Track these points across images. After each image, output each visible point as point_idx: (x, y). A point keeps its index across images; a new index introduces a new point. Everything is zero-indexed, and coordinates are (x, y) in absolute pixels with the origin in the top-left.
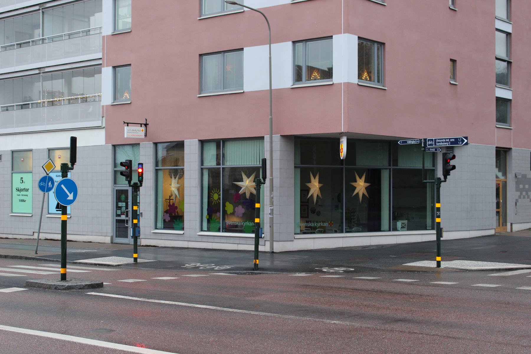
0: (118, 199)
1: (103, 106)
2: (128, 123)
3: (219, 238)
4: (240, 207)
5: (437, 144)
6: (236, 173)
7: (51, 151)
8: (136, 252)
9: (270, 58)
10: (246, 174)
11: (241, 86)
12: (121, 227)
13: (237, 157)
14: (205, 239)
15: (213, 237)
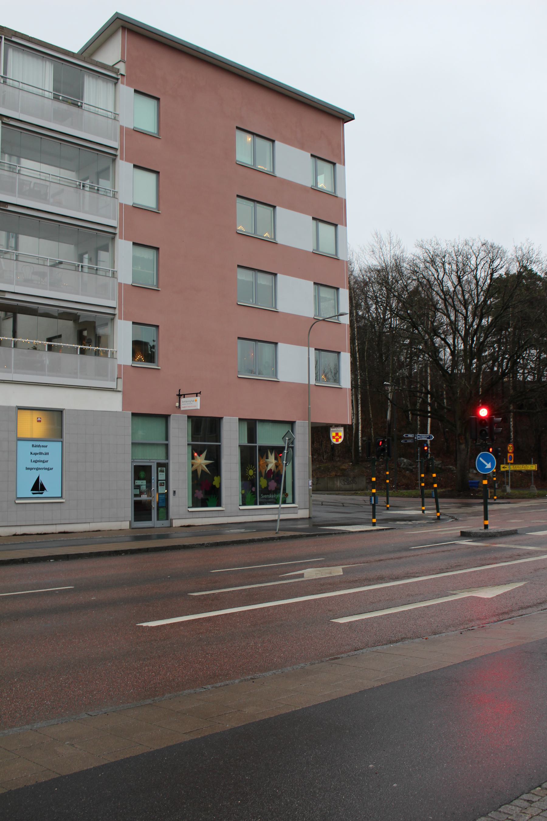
0: (137, 477)
1: (119, 366)
2: (184, 395)
4: (273, 481)
6: (264, 451)
7: (60, 413)
8: (374, 518)
9: (309, 358)
11: (276, 376)
12: (141, 510)
13: (267, 437)
14: (247, 513)
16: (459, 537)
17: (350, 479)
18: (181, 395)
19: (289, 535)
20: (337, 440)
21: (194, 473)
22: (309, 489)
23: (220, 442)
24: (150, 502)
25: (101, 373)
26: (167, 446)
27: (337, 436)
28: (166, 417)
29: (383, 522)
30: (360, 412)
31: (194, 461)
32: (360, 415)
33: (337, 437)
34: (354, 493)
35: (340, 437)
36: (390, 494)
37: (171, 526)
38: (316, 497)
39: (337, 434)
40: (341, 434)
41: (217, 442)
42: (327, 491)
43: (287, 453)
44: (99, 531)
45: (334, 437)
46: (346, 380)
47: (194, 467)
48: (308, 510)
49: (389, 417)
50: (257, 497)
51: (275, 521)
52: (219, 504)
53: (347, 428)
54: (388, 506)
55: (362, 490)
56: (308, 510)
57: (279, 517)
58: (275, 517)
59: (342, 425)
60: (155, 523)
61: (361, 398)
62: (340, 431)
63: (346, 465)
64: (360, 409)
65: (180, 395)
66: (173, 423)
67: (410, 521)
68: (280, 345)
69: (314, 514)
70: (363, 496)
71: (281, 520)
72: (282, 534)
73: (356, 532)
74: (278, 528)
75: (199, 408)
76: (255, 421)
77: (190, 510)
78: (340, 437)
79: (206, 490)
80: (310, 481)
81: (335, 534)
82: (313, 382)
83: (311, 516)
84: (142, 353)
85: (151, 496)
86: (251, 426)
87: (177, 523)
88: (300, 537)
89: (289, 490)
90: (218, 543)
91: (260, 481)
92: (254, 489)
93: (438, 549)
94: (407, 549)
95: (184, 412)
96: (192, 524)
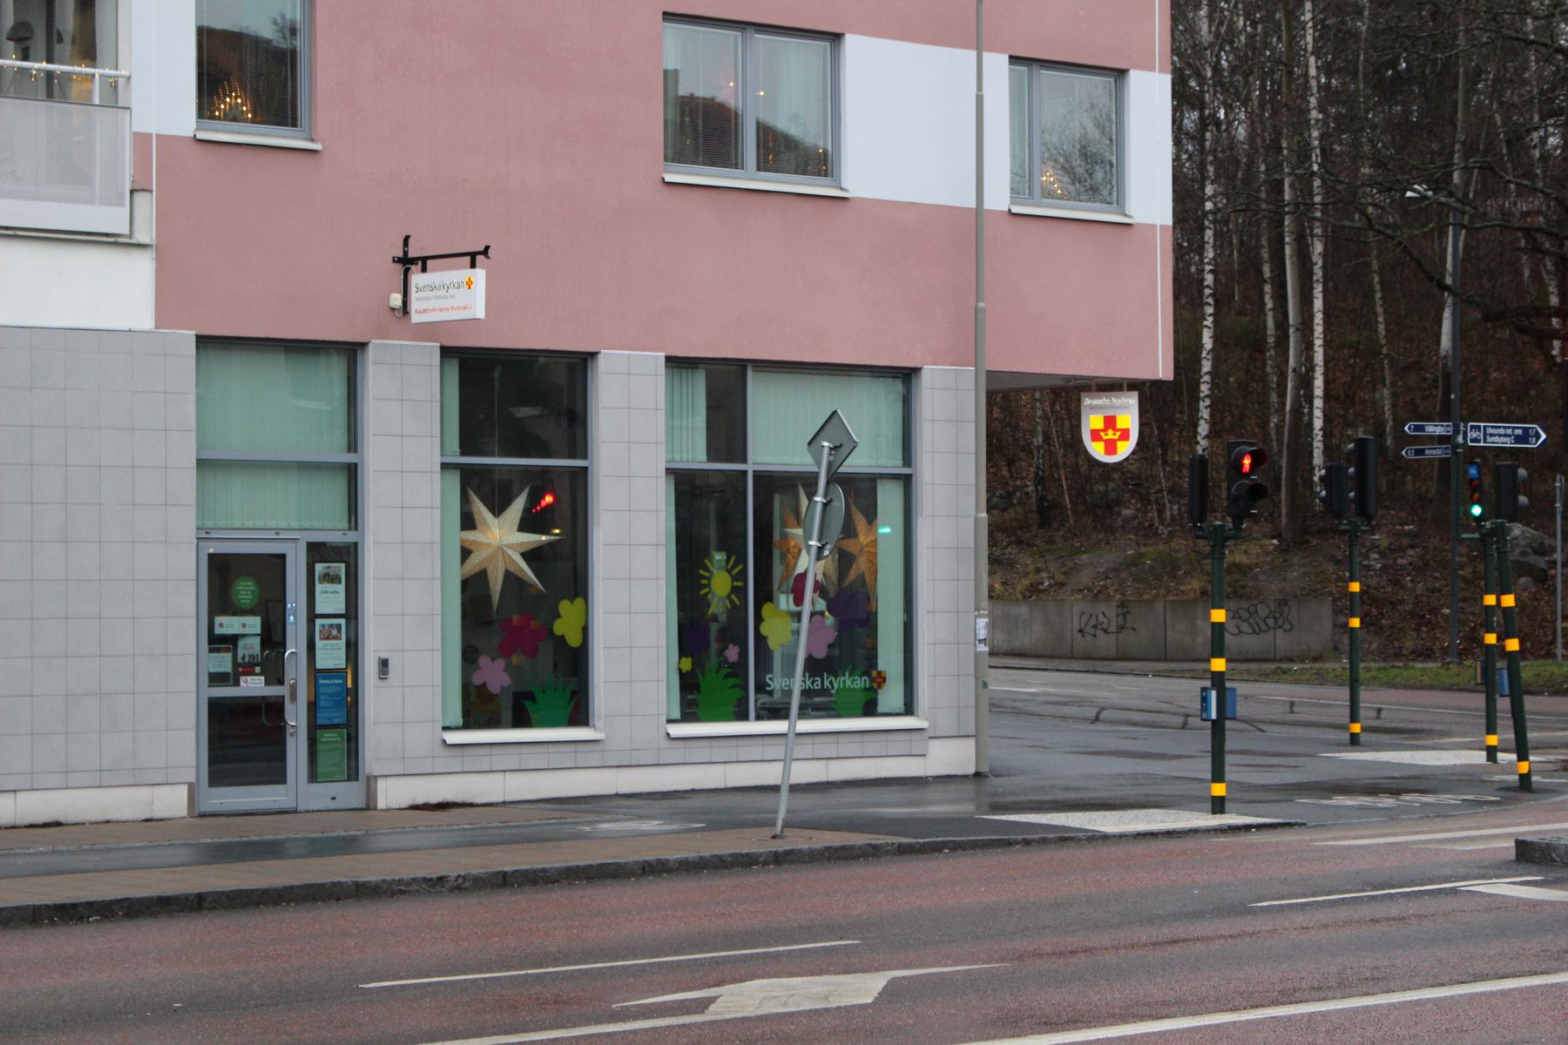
0: (220, 599)
1: (142, 140)
2: (424, 260)
3: (759, 741)
5: (1489, 439)
8: (1218, 776)
9: (980, 100)
10: (483, 499)
12: (241, 737)
13: (779, 435)
14: (701, 752)
15: (733, 742)
16: (1507, 864)
17: (1263, 611)
18: (413, 261)
19: (820, 846)
20: (1111, 448)
21: (474, 589)
22: (977, 655)
23: (585, 456)
24: (275, 708)
25: (71, 174)
26: (352, 473)
27: (1112, 431)
28: (352, 352)
29: (1275, 796)
30: (1319, 318)
31: (471, 535)
32: (1318, 330)
33: (1110, 435)
34: (1274, 672)
35: (1125, 435)
36: (1363, 675)
37: (370, 806)
38: (1007, 683)
39: (1110, 422)
40: (1129, 419)
41: (572, 456)
42: (1166, 660)
43: (825, 505)
44: (58, 824)
45: (1096, 435)
46: (1149, 194)
47: (474, 563)
48: (972, 742)
49: (1446, 341)
50: (746, 688)
51: (775, 789)
52: (579, 714)
53: (1151, 395)
54: (1356, 728)
55: (1316, 659)
56: (972, 742)
57: (786, 771)
58: (769, 774)
59: (1133, 385)
60: (297, 790)
61: (1325, 255)
62: (1125, 408)
63: (1253, 548)
64: (1318, 304)
65: (406, 262)
66: (376, 378)
67: (1395, 792)
68: (851, 42)
69: (1003, 754)
70: (1309, 682)
71: (794, 788)
72: (800, 841)
73: (1121, 837)
74: (782, 815)
75: (481, 314)
76: (740, 367)
77: (454, 737)
78: (1125, 435)
79: (523, 655)
80: (982, 622)
81: (1027, 843)
82: (998, 198)
83: (984, 769)
84: (243, 88)
85: (281, 682)
86: (723, 387)
87: (392, 794)
88: (872, 853)
89: (889, 658)
90: (505, 874)
91: (759, 619)
92: (732, 653)
93: (1378, 911)
94: (1244, 910)
95: (427, 331)
96: (459, 799)
